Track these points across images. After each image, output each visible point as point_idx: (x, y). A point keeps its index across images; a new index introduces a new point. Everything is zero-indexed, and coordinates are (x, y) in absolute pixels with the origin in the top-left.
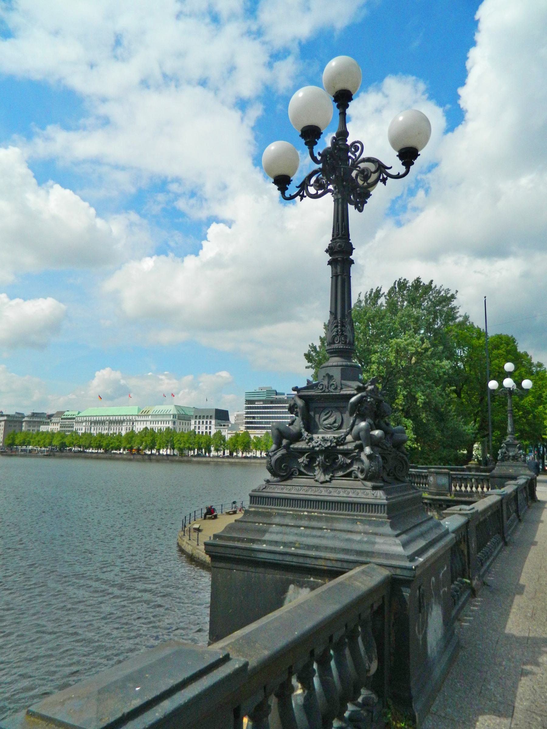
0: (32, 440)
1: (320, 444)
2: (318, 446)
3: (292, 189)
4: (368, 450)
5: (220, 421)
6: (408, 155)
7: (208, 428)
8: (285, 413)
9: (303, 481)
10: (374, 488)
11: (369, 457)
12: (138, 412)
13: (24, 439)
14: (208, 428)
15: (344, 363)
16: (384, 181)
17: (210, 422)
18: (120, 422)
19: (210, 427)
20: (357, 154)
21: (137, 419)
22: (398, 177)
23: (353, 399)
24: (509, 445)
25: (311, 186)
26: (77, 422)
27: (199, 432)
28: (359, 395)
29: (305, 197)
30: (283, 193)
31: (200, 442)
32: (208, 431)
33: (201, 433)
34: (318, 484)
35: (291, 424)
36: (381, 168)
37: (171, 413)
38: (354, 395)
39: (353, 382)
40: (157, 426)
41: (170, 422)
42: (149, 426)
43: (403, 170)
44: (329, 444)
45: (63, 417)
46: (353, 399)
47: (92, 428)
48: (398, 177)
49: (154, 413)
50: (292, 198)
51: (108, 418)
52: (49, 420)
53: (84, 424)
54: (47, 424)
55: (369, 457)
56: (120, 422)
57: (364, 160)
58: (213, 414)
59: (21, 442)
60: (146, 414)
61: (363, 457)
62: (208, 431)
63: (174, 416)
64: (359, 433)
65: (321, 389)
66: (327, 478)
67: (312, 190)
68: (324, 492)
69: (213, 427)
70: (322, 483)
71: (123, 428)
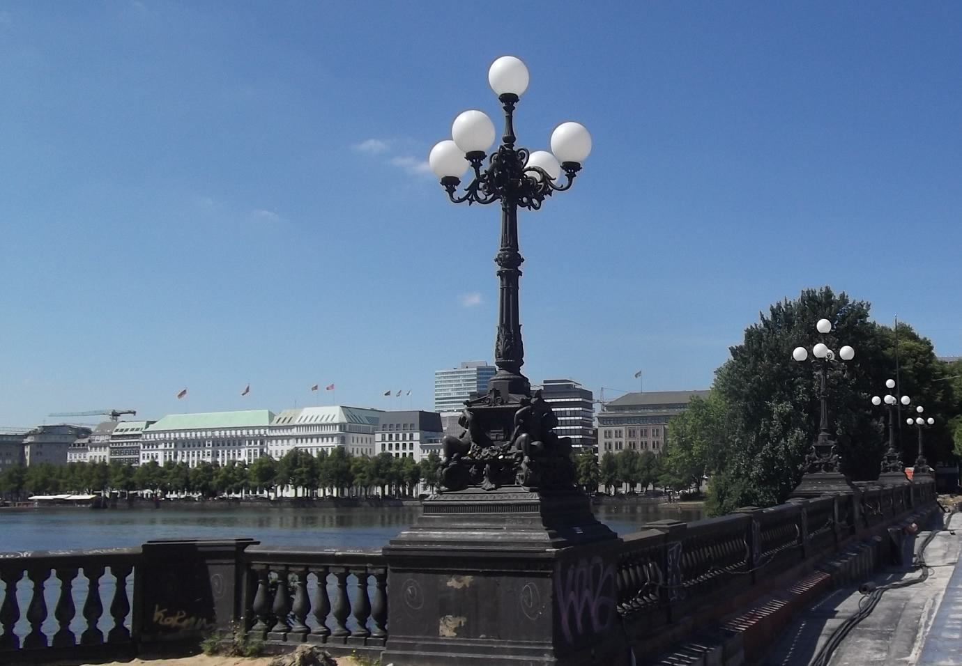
0: (61, 481)
1: (488, 454)
2: (486, 457)
3: (461, 192)
4: (526, 458)
5: (427, 433)
7: (408, 446)
8: (564, 414)
9: (471, 489)
10: (531, 491)
11: (527, 464)
12: (271, 419)
13: (44, 480)
14: (408, 446)
15: (511, 377)
17: (411, 436)
18: (236, 442)
19: (411, 445)
21: (269, 433)
23: (518, 412)
24: (890, 459)
25: (480, 190)
26: (148, 444)
27: (397, 455)
28: (525, 408)
29: (474, 201)
30: (451, 196)
31: (401, 475)
32: (408, 452)
33: (401, 456)
34: (485, 491)
35: (462, 436)
37: (336, 420)
38: (518, 409)
39: (517, 396)
40: (313, 447)
41: (335, 439)
42: (301, 445)
43: (566, 182)
44: (496, 453)
45: (114, 434)
46: (518, 412)
47: (179, 453)
49: (301, 422)
50: (460, 200)
51: (209, 434)
52: (86, 441)
53: (161, 447)
54: (83, 448)
55: (527, 464)
56: (236, 442)
57: (530, 169)
58: (417, 422)
59: (40, 484)
60: (285, 423)
61: (523, 465)
62: (408, 452)
63: (342, 426)
64: (520, 444)
65: (488, 404)
66: (493, 486)
68: (490, 497)
69: (417, 445)
70: (488, 490)
71: (243, 451)
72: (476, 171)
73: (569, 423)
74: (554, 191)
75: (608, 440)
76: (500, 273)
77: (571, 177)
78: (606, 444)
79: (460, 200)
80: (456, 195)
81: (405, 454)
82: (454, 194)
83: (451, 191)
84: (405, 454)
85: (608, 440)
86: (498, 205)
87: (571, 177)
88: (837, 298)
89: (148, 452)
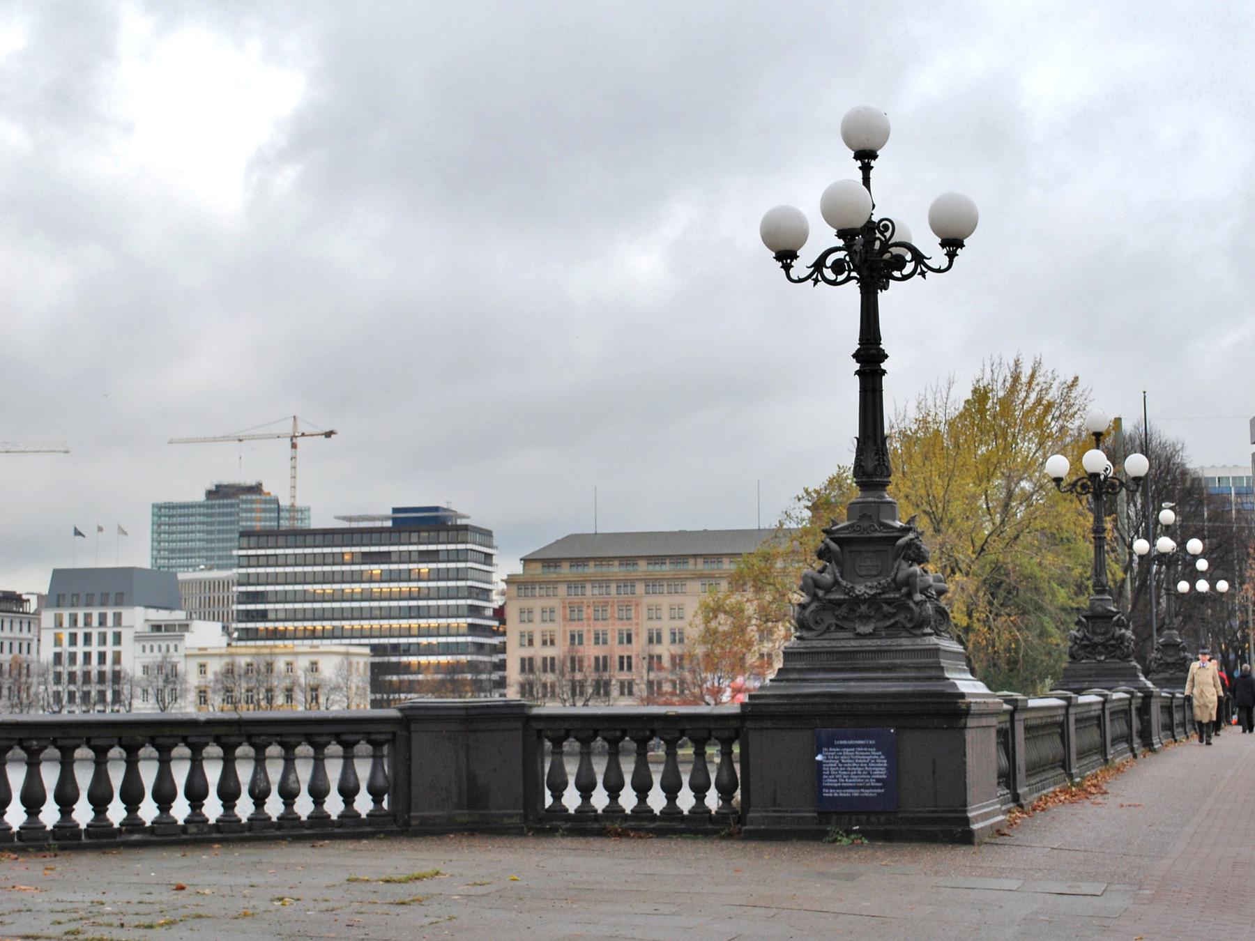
3: (801, 267)
6: (952, 244)
14: (95, 639)
16: (923, 274)
20: (888, 234)
22: (939, 271)
36: (919, 258)
43: (944, 262)
48: (939, 271)
50: (800, 281)
67: (829, 274)
72: (877, 339)
73: (272, 560)
74: (929, 274)
75: (527, 627)
76: (857, 373)
77: (951, 256)
78: (522, 636)
79: (800, 281)
80: (794, 273)
81: (75, 654)
82: (791, 271)
83: (787, 268)
84: (75, 654)
85: (527, 627)
86: (853, 289)
87: (951, 256)
88: (914, 427)
89: (12, 635)
